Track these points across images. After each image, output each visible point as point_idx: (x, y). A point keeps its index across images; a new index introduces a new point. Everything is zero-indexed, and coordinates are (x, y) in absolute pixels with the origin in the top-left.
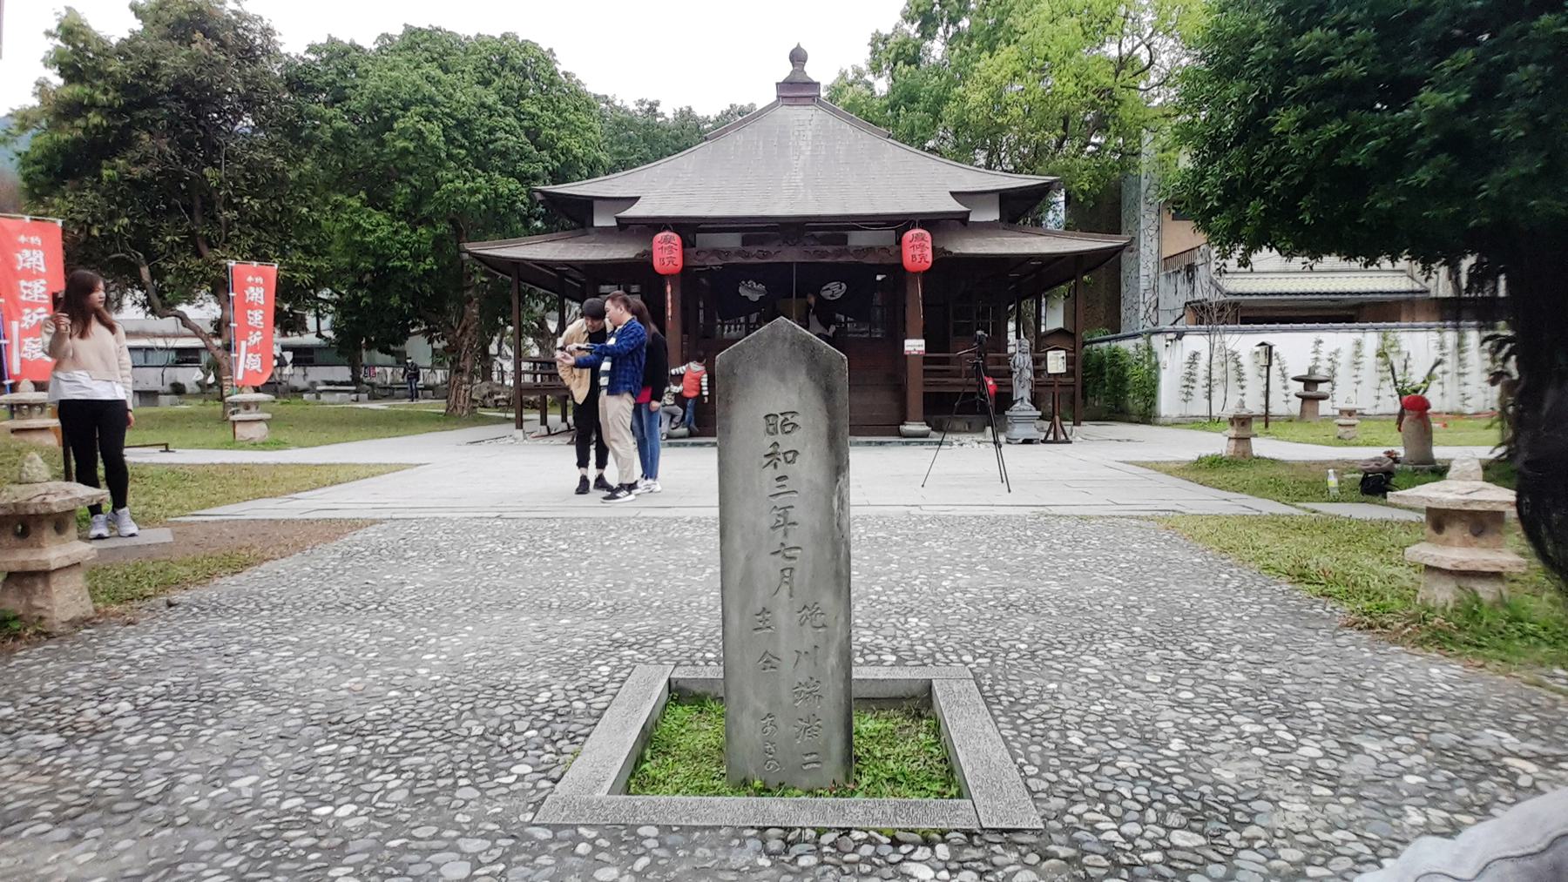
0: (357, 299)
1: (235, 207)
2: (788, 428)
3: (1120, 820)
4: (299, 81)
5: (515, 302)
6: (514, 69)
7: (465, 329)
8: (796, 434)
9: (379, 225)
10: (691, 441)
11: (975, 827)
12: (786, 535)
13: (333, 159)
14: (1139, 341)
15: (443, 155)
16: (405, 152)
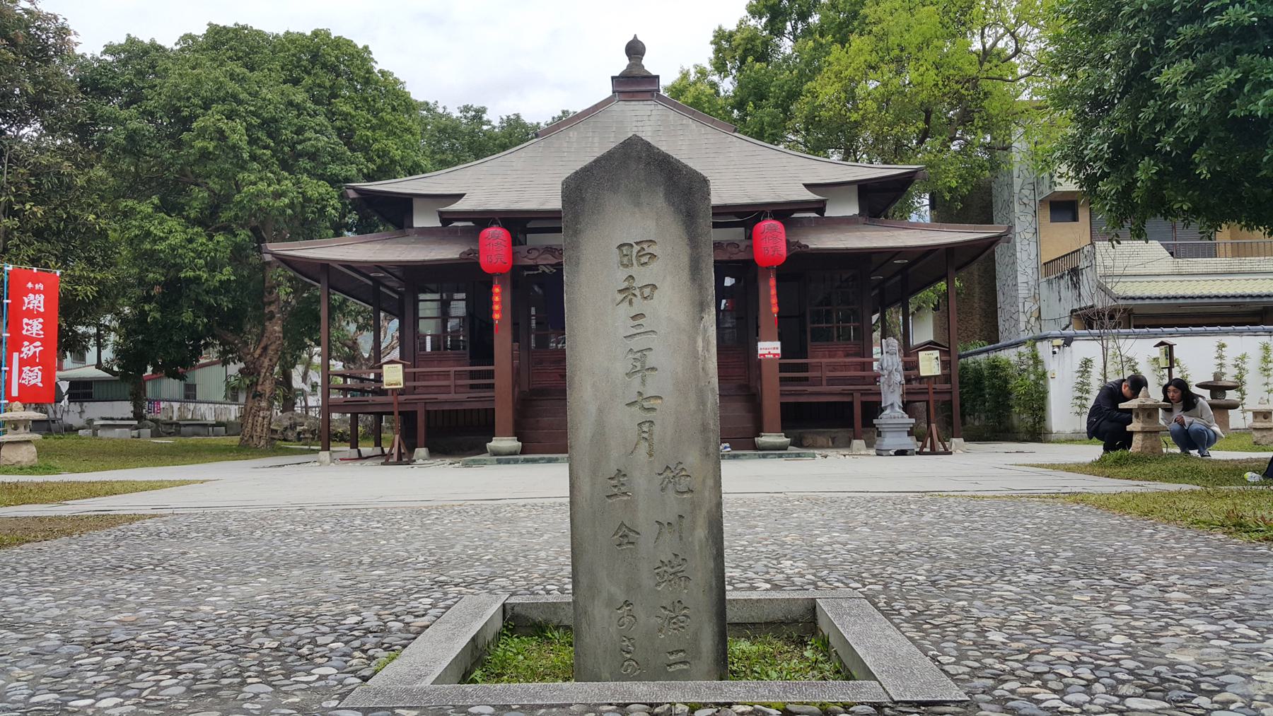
0: (144, 314)
1: (15, 214)
2: (644, 259)
3: (1061, 693)
4: (96, 82)
5: (324, 314)
6: (327, 68)
7: (265, 349)
8: (655, 266)
9: (171, 232)
10: (522, 457)
11: (884, 699)
12: (643, 382)
13: (125, 164)
14: (1022, 349)
15: (246, 156)
16: (205, 155)
